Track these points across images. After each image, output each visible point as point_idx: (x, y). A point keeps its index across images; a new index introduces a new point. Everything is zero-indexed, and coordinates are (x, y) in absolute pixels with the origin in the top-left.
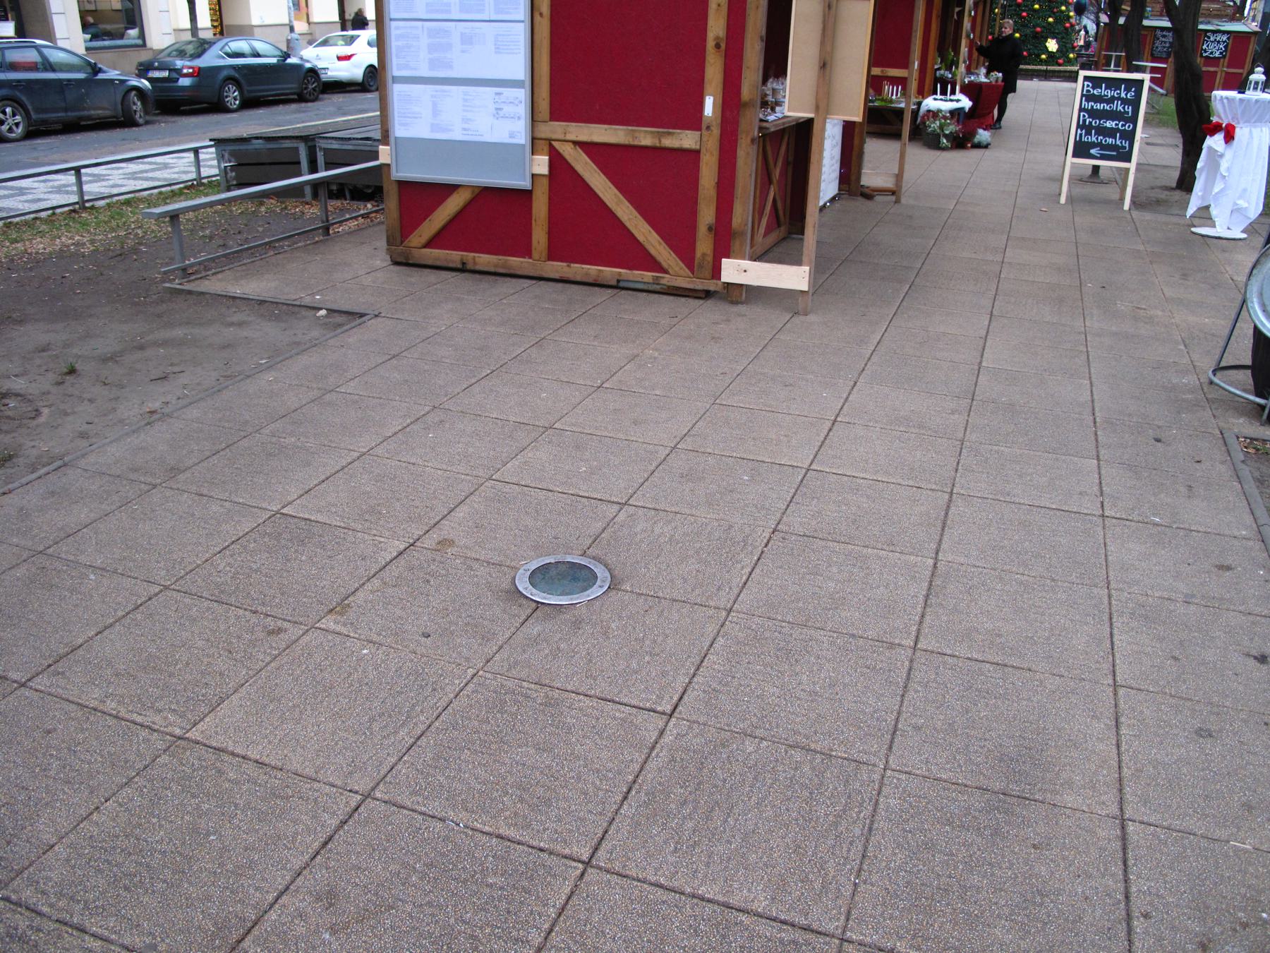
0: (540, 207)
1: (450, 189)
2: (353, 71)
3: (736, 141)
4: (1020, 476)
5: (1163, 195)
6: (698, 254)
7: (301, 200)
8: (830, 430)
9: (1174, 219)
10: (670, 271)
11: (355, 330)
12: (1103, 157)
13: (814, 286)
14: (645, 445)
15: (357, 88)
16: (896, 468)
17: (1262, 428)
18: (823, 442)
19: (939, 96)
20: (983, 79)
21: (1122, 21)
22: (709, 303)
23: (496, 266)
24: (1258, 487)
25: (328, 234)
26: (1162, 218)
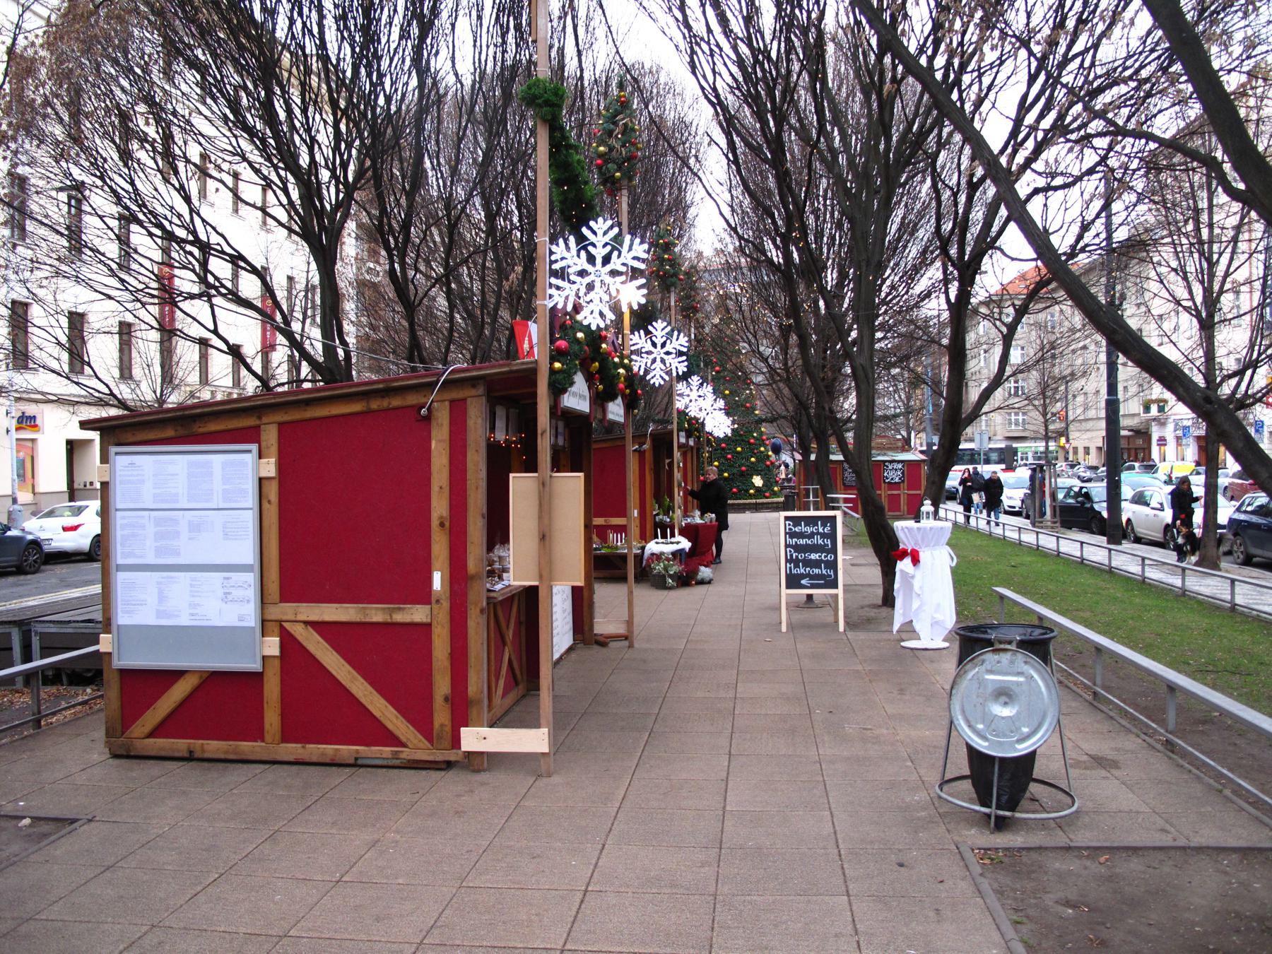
0: (272, 688)
1: (176, 675)
2: (81, 540)
3: (465, 612)
4: (776, 926)
5: (873, 613)
6: (436, 725)
7: (11, 688)
8: (582, 902)
9: (885, 636)
10: (409, 744)
11: (63, 840)
12: (813, 586)
13: (555, 745)
14: (389, 945)
15: (83, 557)
16: (652, 935)
17: (992, 836)
18: (576, 917)
19: (660, 540)
20: (698, 521)
21: (813, 457)
22: (451, 775)
23: (227, 752)
24: (999, 899)
25: (39, 726)
26: (874, 636)
